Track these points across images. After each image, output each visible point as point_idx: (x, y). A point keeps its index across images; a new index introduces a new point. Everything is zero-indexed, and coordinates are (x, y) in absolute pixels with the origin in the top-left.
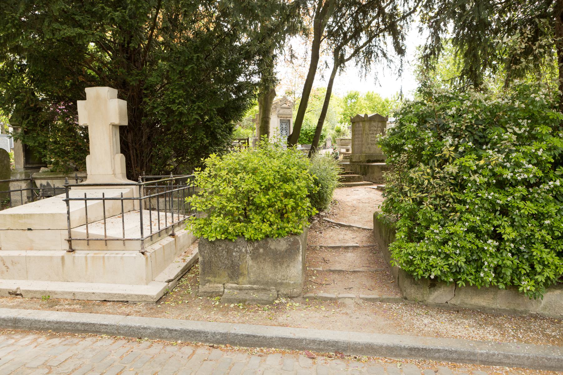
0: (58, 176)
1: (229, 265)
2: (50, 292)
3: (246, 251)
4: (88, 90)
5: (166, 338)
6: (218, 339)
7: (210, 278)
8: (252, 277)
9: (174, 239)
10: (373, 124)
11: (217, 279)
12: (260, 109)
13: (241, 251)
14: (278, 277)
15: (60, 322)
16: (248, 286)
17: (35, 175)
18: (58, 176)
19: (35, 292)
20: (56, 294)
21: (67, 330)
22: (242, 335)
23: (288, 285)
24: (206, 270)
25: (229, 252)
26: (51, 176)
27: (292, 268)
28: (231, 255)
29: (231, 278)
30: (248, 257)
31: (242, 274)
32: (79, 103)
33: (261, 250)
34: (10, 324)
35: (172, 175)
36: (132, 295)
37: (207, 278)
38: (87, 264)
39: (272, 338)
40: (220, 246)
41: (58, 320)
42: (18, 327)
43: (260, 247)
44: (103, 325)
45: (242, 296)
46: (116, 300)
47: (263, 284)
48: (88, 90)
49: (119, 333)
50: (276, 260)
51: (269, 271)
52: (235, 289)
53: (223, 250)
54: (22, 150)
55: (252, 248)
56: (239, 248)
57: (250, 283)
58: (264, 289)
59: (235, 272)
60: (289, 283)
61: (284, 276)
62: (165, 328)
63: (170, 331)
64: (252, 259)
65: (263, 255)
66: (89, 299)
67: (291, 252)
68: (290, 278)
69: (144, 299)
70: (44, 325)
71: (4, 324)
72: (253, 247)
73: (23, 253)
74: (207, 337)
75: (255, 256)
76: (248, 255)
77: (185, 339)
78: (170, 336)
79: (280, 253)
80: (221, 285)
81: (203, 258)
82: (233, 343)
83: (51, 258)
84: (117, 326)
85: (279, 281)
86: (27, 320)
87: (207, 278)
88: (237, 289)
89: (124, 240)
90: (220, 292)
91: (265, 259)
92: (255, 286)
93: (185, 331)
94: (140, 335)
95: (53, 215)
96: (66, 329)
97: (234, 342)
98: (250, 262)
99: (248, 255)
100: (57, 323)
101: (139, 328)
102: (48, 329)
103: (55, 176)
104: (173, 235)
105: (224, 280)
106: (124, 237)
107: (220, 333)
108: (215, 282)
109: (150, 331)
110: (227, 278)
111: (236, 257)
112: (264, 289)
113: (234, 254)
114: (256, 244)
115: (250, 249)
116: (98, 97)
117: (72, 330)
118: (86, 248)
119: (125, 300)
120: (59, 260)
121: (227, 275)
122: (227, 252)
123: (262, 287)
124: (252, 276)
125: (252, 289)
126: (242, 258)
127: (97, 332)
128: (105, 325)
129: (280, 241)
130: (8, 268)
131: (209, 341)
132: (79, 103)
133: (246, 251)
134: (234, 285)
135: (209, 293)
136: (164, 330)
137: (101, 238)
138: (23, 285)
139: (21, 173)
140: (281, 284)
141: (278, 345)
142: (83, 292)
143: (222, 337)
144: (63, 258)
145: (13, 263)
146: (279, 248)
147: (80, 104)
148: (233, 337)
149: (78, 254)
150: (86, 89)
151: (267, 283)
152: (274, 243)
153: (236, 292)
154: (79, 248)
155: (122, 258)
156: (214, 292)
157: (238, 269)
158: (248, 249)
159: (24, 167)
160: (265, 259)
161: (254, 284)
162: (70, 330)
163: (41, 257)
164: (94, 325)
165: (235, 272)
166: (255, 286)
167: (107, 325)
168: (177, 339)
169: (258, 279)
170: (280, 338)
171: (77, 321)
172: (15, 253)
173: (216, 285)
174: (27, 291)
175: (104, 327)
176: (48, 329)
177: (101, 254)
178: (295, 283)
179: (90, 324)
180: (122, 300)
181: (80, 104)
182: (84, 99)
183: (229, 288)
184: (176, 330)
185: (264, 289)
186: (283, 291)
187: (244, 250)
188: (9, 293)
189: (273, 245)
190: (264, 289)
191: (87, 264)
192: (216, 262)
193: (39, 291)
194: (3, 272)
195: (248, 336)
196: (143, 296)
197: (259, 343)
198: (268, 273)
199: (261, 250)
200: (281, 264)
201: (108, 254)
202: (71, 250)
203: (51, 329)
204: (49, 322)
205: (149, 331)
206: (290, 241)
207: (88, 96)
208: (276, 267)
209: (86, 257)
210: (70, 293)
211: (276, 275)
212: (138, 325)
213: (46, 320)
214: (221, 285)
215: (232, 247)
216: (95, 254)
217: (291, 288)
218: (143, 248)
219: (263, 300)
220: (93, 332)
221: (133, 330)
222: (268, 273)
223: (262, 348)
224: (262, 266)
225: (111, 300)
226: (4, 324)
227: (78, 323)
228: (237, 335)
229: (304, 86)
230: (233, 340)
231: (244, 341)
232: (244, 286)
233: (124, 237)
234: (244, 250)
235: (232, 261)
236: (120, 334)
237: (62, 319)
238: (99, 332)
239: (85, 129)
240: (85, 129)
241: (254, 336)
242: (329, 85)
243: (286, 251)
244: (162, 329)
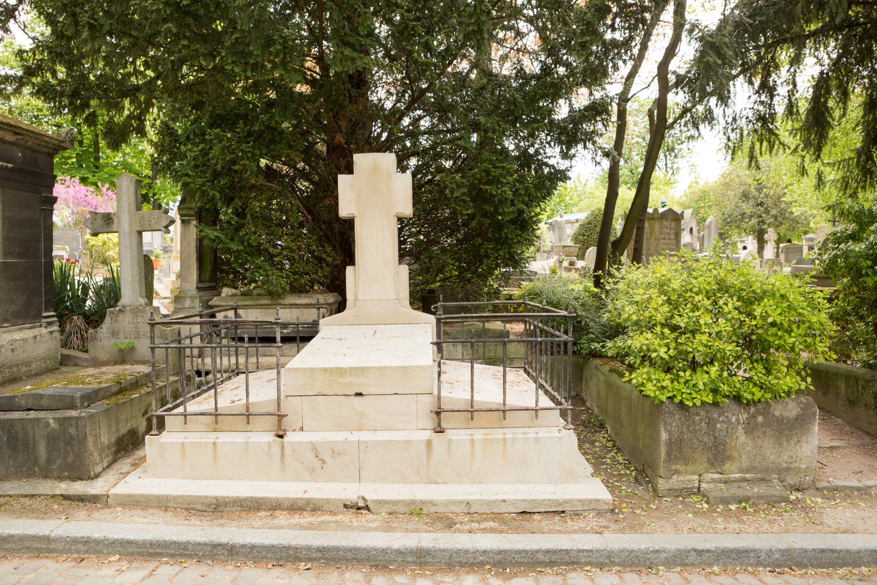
0: (260, 302)
2: (423, 502)
4: (357, 158)
5: (693, 564)
6: (777, 559)
7: (678, 467)
8: (745, 462)
10: (665, 223)
11: (689, 468)
13: (729, 420)
14: (784, 459)
15: (506, 551)
16: (737, 475)
17: (215, 301)
18: (260, 302)
19: (395, 503)
20: (435, 505)
21: (518, 564)
22: (814, 550)
23: (798, 470)
24: (674, 453)
25: (711, 423)
26: (246, 303)
27: (804, 444)
28: (714, 428)
29: (712, 464)
30: (740, 430)
31: (729, 458)
32: (342, 178)
33: (760, 419)
34: (410, 559)
36: (572, 500)
37: (674, 467)
38: (473, 452)
39: (859, 552)
40: (698, 414)
41: (502, 548)
42: (426, 563)
43: (759, 413)
44: (583, 551)
45: (734, 491)
46: (543, 510)
47: (761, 471)
48: (357, 158)
49: (611, 562)
50: (780, 433)
51: (770, 452)
52: (717, 482)
54: (195, 257)
55: (745, 416)
57: (741, 471)
58: (762, 480)
59: (718, 454)
60: (799, 468)
61: (792, 458)
62: (690, 548)
63: (699, 552)
64: (746, 433)
65: (762, 425)
66: (496, 510)
67: (803, 420)
68: (801, 459)
69: (592, 506)
70: (475, 558)
71: (400, 559)
72: (749, 413)
73: (337, 436)
74: (759, 557)
75: (751, 428)
76: (740, 427)
77: (724, 564)
78: (699, 560)
79: (788, 422)
80: (696, 477)
81: (670, 435)
82: (801, 565)
83: (408, 443)
84: (608, 551)
85: (785, 465)
86: (444, 550)
87: (674, 467)
88: (720, 481)
89: (504, 411)
90: (694, 487)
91: (764, 433)
92: (748, 476)
93: (723, 551)
94: (648, 563)
95: (404, 369)
96: (517, 562)
97: (801, 563)
98: (743, 438)
99: (740, 427)
100: (500, 552)
101: (645, 552)
102: (482, 564)
103: (254, 303)
105: (701, 468)
106: (537, 405)
107: (780, 550)
108: (686, 472)
109: (666, 555)
110: (706, 465)
111: (721, 430)
112: (762, 480)
113: (718, 426)
114: (753, 409)
115: (743, 417)
116: (376, 169)
117: (528, 563)
118: (463, 426)
119: (560, 509)
120: (423, 448)
121: (706, 460)
122: (708, 424)
123: (759, 476)
124: (743, 460)
125: (745, 480)
126: (730, 431)
127: (573, 563)
128: (587, 551)
129: (787, 403)
130: (324, 462)
131: (762, 564)
132: (342, 178)
133: (738, 420)
134: (717, 476)
135: (676, 490)
136: (689, 552)
137: (497, 407)
138: (372, 492)
139: (193, 298)
140: (788, 469)
141: (869, 563)
142: (485, 500)
143: (783, 556)
144: (429, 443)
145: (334, 453)
146: (786, 414)
147: (343, 180)
148: (800, 554)
149: (451, 434)
151: (766, 470)
152: (780, 407)
153: (722, 486)
154: (449, 426)
155: (537, 440)
156: (684, 488)
157: (724, 450)
159: (197, 288)
160: (764, 433)
161: (748, 471)
162: (524, 563)
163: (389, 442)
164: (567, 552)
165: (718, 454)
166: (748, 476)
167: (591, 551)
168: (711, 565)
169: (754, 464)
170: (871, 551)
171: (536, 547)
172: (337, 436)
173: (688, 477)
174: (380, 503)
175: (586, 554)
176: (482, 564)
177: (498, 434)
178: (808, 467)
179: (560, 551)
180: (554, 509)
181: (343, 180)
182: (351, 172)
183: (710, 480)
184: (708, 551)
185: (762, 480)
186: (791, 480)
187: (734, 419)
188: (345, 506)
189: (778, 410)
190: (762, 480)
191: (473, 452)
192: (690, 440)
193: (403, 501)
194: (313, 470)
195: (823, 551)
196: (590, 501)
197: (840, 561)
198: (769, 454)
199: (760, 419)
200: (789, 439)
201: (509, 434)
202: (439, 430)
203: (488, 563)
204: (485, 552)
205: (664, 555)
206: (802, 402)
207: (356, 168)
208: (780, 444)
209: (472, 441)
210: (460, 502)
211: (780, 456)
212: (643, 547)
213: (479, 548)
214: (696, 477)
215: (715, 416)
216: (486, 434)
217: (802, 475)
218: (279, 428)
219: (775, 496)
220: (567, 564)
221: (637, 556)
222: (769, 454)
223: (850, 568)
224: (760, 443)
225: (535, 510)
226: (400, 559)
227: (538, 551)
228: (806, 551)
230: (800, 560)
231: (816, 559)
232: (732, 476)
233: (537, 405)
234: (734, 419)
235: (715, 438)
236: (613, 563)
237: (508, 546)
238: (577, 563)
239: (349, 223)
240: (349, 223)
241: (832, 551)
243: (796, 419)
244: (685, 551)
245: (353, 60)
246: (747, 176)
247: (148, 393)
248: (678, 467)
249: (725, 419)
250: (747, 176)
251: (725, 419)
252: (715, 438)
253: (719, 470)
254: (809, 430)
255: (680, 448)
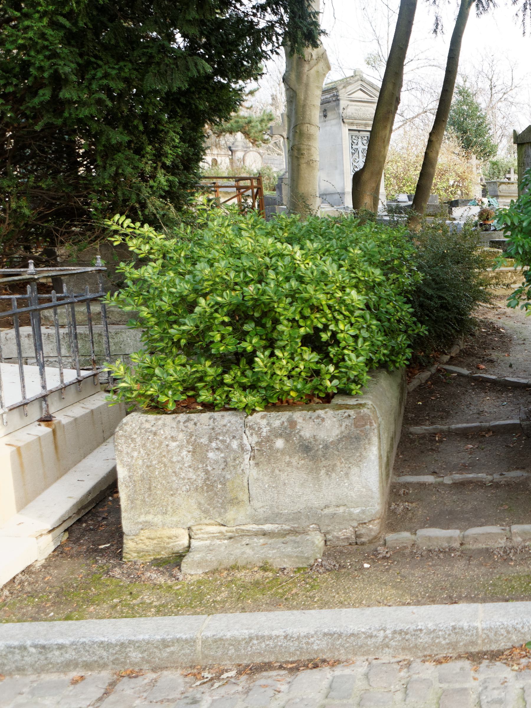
1: (200, 483)
3: (242, 446)
8: (261, 505)
9: (49, 430)
12: (432, 180)
13: (228, 447)
28: (204, 459)
35: (31, 268)
37: (142, 518)
47: (287, 520)
53: (181, 447)
56: (223, 441)
65: (283, 452)
76: (247, 457)
98: (253, 473)
104: (47, 420)
111: (216, 462)
146: (322, 435)
150: (240, 133)
158: (245, 441)
161: (267, 520)
166: (267, 527)
187: (235, 444)
208: (318, 479)
229: (397, 16)
234: (235, 444)
235: (207, 472)
242: (451, 51)
245: (54, 55)
246: (494, 215)
247: (435, 215)
248: (149, 518)
249: (220, 445)
250: (494, 215)
251: (220, 445)
252: (207, 472)
253: (219, 520)
254: (361, 459)
255: (150, 489)
